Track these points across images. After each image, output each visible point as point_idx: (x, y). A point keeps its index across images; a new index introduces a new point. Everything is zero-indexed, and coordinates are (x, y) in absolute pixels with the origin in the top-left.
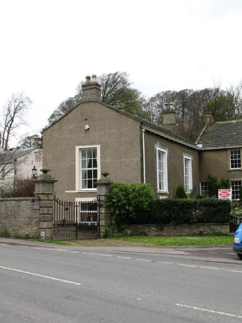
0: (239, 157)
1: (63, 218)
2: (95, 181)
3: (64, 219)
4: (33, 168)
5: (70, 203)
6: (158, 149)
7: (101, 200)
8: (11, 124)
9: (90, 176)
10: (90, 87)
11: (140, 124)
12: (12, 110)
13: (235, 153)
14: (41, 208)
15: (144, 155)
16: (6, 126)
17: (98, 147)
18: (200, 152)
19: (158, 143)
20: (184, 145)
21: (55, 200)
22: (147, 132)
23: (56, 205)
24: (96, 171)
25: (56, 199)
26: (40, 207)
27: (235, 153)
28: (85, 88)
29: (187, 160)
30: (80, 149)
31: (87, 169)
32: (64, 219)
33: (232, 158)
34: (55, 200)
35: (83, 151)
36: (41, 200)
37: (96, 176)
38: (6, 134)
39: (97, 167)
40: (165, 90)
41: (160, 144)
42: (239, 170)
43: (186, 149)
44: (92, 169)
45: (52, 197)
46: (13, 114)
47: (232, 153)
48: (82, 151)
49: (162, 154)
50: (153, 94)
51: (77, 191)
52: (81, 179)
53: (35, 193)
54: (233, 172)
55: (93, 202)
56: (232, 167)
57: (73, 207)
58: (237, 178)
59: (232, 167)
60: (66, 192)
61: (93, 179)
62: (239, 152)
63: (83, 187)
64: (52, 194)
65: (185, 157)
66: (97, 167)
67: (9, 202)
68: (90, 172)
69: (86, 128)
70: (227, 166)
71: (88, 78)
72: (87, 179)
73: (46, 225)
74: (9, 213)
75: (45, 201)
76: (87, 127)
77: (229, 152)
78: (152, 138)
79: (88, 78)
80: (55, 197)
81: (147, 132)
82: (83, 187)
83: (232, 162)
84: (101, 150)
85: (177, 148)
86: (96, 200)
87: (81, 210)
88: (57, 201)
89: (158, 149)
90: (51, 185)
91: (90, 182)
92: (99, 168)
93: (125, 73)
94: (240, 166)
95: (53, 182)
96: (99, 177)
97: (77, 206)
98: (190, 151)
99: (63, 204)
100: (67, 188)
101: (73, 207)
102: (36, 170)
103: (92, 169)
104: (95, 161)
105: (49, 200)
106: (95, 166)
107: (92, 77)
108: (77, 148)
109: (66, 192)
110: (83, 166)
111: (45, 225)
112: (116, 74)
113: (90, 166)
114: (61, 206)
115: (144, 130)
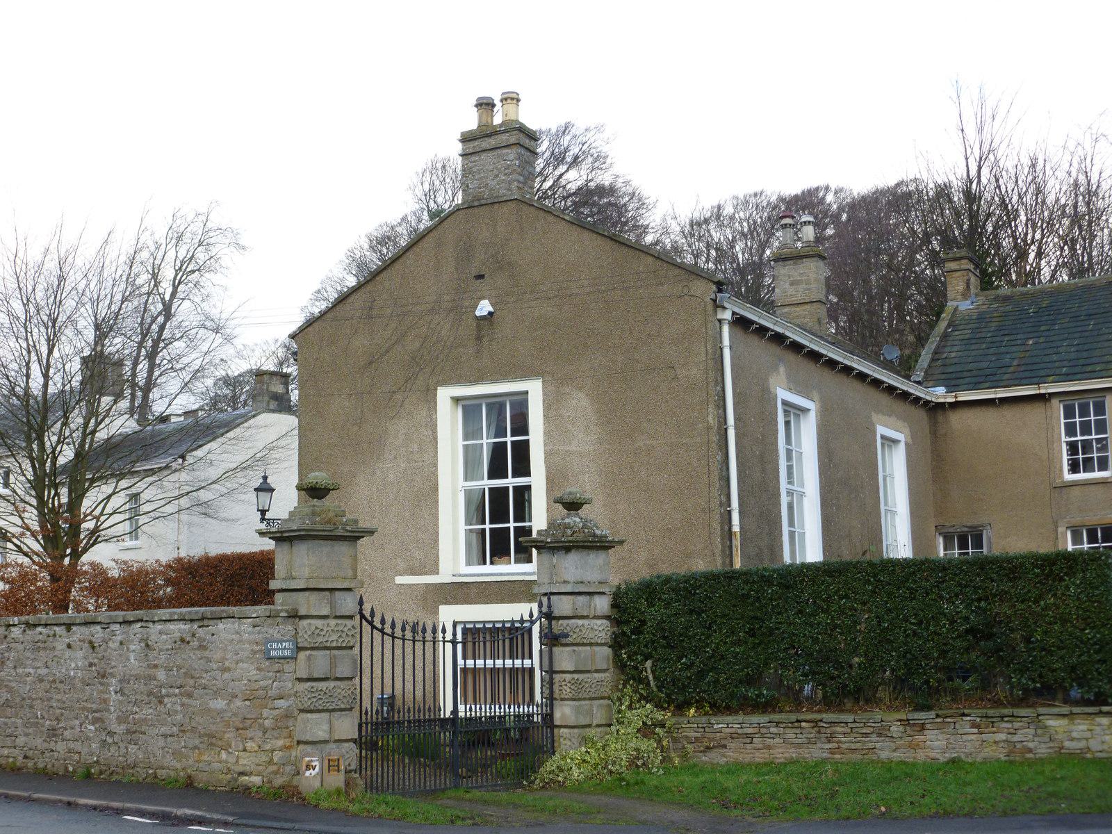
0: (1101, 427)
1: (388, 691)
2: (524, 532)
3: (393, 697)
4: (258, 482)
5: (414, 630)
6: (783, 394)
7: (556, 613)
8: (162, 327)
9: (499, 514)
10: (492, 142)
11: (714, 288)
12: (168, 273)
13: (1084, 412)
14: (302, 655)
15: (731, 420)
16: (144, 336)
17: (534, 390)
18: (935, 409)
19: (782, 369)
20: (877, 383)
21: (363, 616)
22: (741, 323)
23: (367, 639)
24: (523, 493)
25: (367, 614)
26: (299, 649)
27: (1084, 412)
28: (472, 146)
29: (890, 442)
30: (456, 400)
31: (487, 483)
32: (393, 697)
33: (1070, 430)
34: (363, 616)
35: (469, 408)
36: (302, 618)
37: (523, 510)
38: (143, 366)
39: (528, 474)
40: (744, 189)
41: (788, 377)
42: (1103, 482)
43: (885, 400)
44: (510, 482)
45: (348, 604)
46: (170, 290)
47: (1069, 413)
48: (465, 408)
49: (797, 416)
50: (687, 211)
51: (445, 576)
52: (462, 527)
53: (274, 585)
54: (1076, 491)
55: (522, 621)
56: (1074, 468)
57: (429, 645)
58: (515, 555)
59: (1074, 468)
60: (400, 580)
61: (1077, 419)
62: (1100, 409)
63: (469, 563)
64: (349, 590)
65: (881, 430)
66: (528, 474)
67: (159, 627)
68: (499, 496)
69: (478, 313)
70: (1051, 464)
71: (485, 105)
72: (488, 526)
73: (326, 727)
74: (161, 675)
75: (319, 623)
76: (484, 307)
77: (1059, 408)
78: (761, 350)
79: (485, 105)
80: (361, 603)
81: (741, 323)
82: (469, 563)
83: (1073, 447)
84: (548, 407)
85: (854, 393)
86: (536, 614)
87: (465, 658)
88: (371, 623)
89: (783, 394)
90: (343, 548)
91: (500, 539)
92: (537, 480)
93: (599, 129)
94: (1103, 465)
95: (353, 537)
96: (539, 520)
97: (393, 636)
98: (900, 407)
99: (398, 633)
100: (402, 565)
101: (429, 645)
102: (272, 490)
103: (510, 482)
104: (522, 451)
105: (337, 617)
106: (523, 467)
107: (503, 100)
108: (445, 395)
109: (400, 580)
110: (470, 471)
111: (317, 727)
112: (566, 129)
113: (497, 470)
114: (399, 642)
115: (727, 315)
